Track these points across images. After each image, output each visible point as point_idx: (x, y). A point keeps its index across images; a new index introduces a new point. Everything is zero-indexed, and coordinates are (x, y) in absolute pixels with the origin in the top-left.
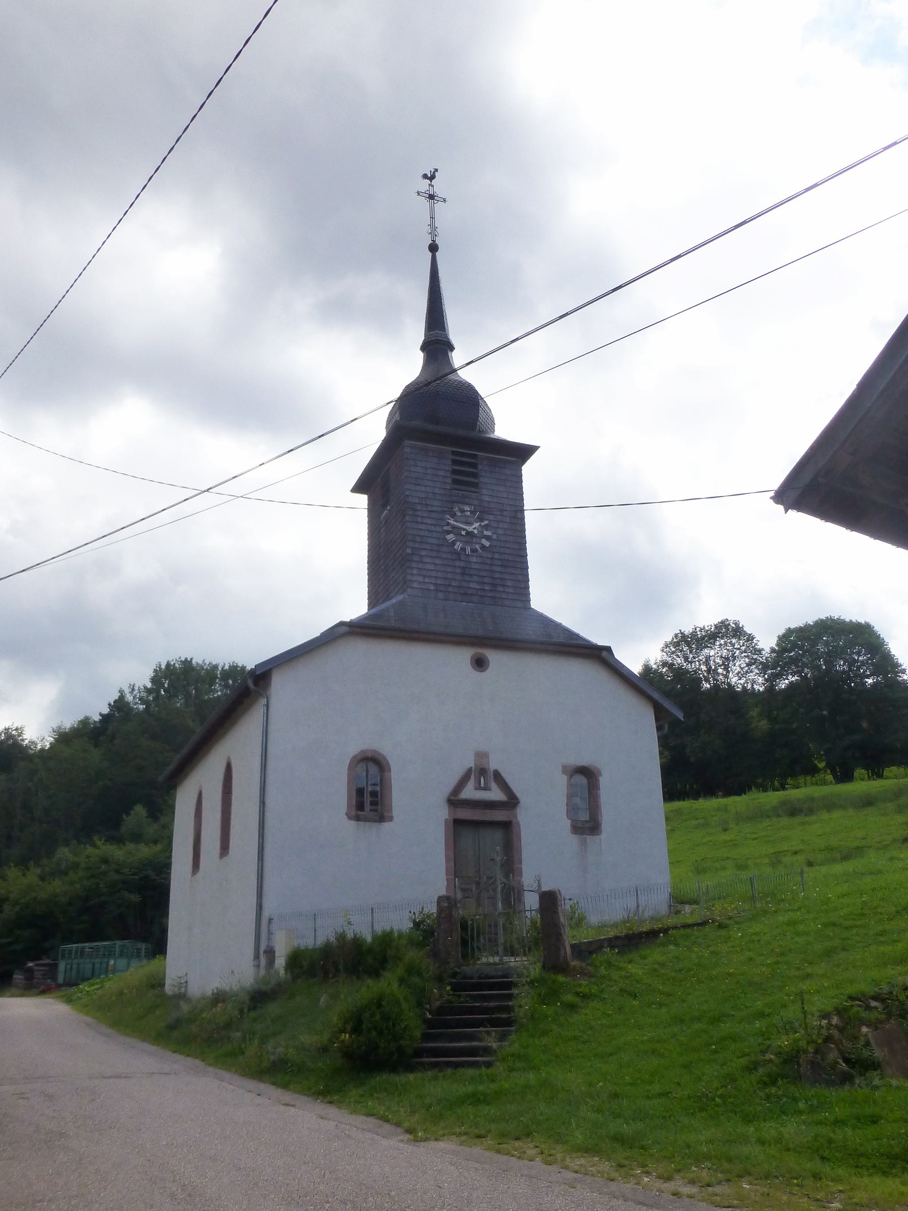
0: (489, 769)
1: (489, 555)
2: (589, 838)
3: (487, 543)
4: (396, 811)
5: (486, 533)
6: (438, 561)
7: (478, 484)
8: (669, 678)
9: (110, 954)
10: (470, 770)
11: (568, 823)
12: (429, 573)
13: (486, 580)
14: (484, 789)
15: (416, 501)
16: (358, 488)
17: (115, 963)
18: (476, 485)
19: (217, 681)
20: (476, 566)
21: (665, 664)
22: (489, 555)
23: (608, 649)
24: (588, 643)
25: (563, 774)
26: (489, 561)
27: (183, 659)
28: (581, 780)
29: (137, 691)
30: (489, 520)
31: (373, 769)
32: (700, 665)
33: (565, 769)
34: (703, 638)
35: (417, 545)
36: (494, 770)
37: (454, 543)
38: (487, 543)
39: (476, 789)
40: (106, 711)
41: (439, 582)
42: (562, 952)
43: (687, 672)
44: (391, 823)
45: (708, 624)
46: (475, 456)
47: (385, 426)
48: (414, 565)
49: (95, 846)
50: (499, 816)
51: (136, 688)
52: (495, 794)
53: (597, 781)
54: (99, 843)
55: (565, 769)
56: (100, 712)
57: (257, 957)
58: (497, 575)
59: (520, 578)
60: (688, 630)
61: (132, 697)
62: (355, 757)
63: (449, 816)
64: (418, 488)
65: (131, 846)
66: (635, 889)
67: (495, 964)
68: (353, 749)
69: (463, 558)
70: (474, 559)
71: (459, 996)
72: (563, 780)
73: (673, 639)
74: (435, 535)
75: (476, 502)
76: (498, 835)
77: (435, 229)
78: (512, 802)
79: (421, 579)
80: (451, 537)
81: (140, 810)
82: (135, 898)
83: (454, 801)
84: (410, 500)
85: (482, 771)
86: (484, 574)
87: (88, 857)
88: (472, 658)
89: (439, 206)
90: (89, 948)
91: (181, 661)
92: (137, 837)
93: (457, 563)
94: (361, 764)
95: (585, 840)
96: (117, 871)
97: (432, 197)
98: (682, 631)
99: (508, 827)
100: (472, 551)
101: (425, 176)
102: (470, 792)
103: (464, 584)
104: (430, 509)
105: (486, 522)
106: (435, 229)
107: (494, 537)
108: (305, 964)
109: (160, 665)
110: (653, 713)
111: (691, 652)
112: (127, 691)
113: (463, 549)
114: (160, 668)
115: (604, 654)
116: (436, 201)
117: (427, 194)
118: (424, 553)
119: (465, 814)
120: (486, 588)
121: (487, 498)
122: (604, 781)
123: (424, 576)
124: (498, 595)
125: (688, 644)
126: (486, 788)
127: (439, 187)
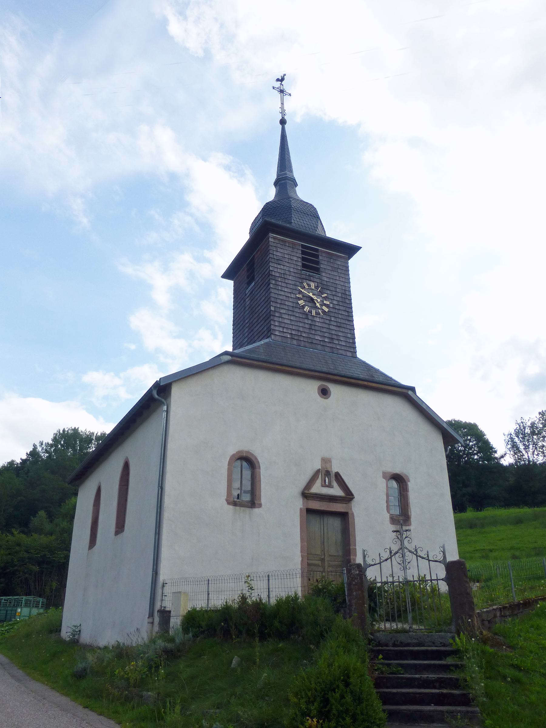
0: (332, 471)
3: (326, 310)
4: (263, 500)
5: (325, 302)
6: (292, 318)
9: (18, 604)
10: (318, 471)
11: (388, 516)
12: (286, 326)
13: (326, 335)
14: (328, 487)
15: (277, 275)
16: (227, 275)
17: (21, 611)
19: (93, 441)
20: (320, 325)
22: (328, 318)
23: (413, 389)
24: (397, 383)
26: (328, 322)
27: (73, 428)
28: (394, 484)
29: (44, 445)
30: (327, 294)
35: (278, 306)
36: (335, 473)
37: (303, 307)
38: (326, 310)
39: (322, 486)
40: (24, 457)
41: (294, 332)
44: (260, 509)
46: (317, 250)
47: (249, 232)
48: (276, 319)
49: (12, 534)
51: (44, 444)
52: (336, 491)
53: (406, 485)
54: (15, 532)
56: (21, 457)
57: (151, 615)
58: (333, 332)
59: (349, 335)
61: (41, 449)
64: (279, 266)
65: (36, 536)
67: (405, 631)
68: (232, 450)
69: (310, 317)
70: (318, 320)
71: (389, 665)
72: (382, 483)
74: (291, 300)
76: (335, 523)
77: (284, 111)
78: (349, 497)
79: (281, 329)
80: (301, 302)
81: (42, 513)
82: (36, 568)
83: (306, 495)
84: (273, 273)
85: (328, 473)
86: (325, 330)
87: (8, 541)
88: (319, 388)
89: (286, 98)
90: (4, 600)
91: (72, 429)
92: (39, 531)
93: (306, 321)
94: (239, 462)
96: (27, 552)
97: (282, 91)
101: (278, 80)
102: (317, 488)
103: (311, 336)
105: (326, 295)
106: (284, 111)
107: (331, 305)
108: (203, 624)
109: (59, 431)
112: (38, 445)
113: (310, 312)
114: (59, 432)
115: (410, 393)
116: (285, 94)
117: (279, 89)
118: (282, 311)
119: (316, 505)
122: (411, 486)
123: (284, 327)
126: (330, 486)
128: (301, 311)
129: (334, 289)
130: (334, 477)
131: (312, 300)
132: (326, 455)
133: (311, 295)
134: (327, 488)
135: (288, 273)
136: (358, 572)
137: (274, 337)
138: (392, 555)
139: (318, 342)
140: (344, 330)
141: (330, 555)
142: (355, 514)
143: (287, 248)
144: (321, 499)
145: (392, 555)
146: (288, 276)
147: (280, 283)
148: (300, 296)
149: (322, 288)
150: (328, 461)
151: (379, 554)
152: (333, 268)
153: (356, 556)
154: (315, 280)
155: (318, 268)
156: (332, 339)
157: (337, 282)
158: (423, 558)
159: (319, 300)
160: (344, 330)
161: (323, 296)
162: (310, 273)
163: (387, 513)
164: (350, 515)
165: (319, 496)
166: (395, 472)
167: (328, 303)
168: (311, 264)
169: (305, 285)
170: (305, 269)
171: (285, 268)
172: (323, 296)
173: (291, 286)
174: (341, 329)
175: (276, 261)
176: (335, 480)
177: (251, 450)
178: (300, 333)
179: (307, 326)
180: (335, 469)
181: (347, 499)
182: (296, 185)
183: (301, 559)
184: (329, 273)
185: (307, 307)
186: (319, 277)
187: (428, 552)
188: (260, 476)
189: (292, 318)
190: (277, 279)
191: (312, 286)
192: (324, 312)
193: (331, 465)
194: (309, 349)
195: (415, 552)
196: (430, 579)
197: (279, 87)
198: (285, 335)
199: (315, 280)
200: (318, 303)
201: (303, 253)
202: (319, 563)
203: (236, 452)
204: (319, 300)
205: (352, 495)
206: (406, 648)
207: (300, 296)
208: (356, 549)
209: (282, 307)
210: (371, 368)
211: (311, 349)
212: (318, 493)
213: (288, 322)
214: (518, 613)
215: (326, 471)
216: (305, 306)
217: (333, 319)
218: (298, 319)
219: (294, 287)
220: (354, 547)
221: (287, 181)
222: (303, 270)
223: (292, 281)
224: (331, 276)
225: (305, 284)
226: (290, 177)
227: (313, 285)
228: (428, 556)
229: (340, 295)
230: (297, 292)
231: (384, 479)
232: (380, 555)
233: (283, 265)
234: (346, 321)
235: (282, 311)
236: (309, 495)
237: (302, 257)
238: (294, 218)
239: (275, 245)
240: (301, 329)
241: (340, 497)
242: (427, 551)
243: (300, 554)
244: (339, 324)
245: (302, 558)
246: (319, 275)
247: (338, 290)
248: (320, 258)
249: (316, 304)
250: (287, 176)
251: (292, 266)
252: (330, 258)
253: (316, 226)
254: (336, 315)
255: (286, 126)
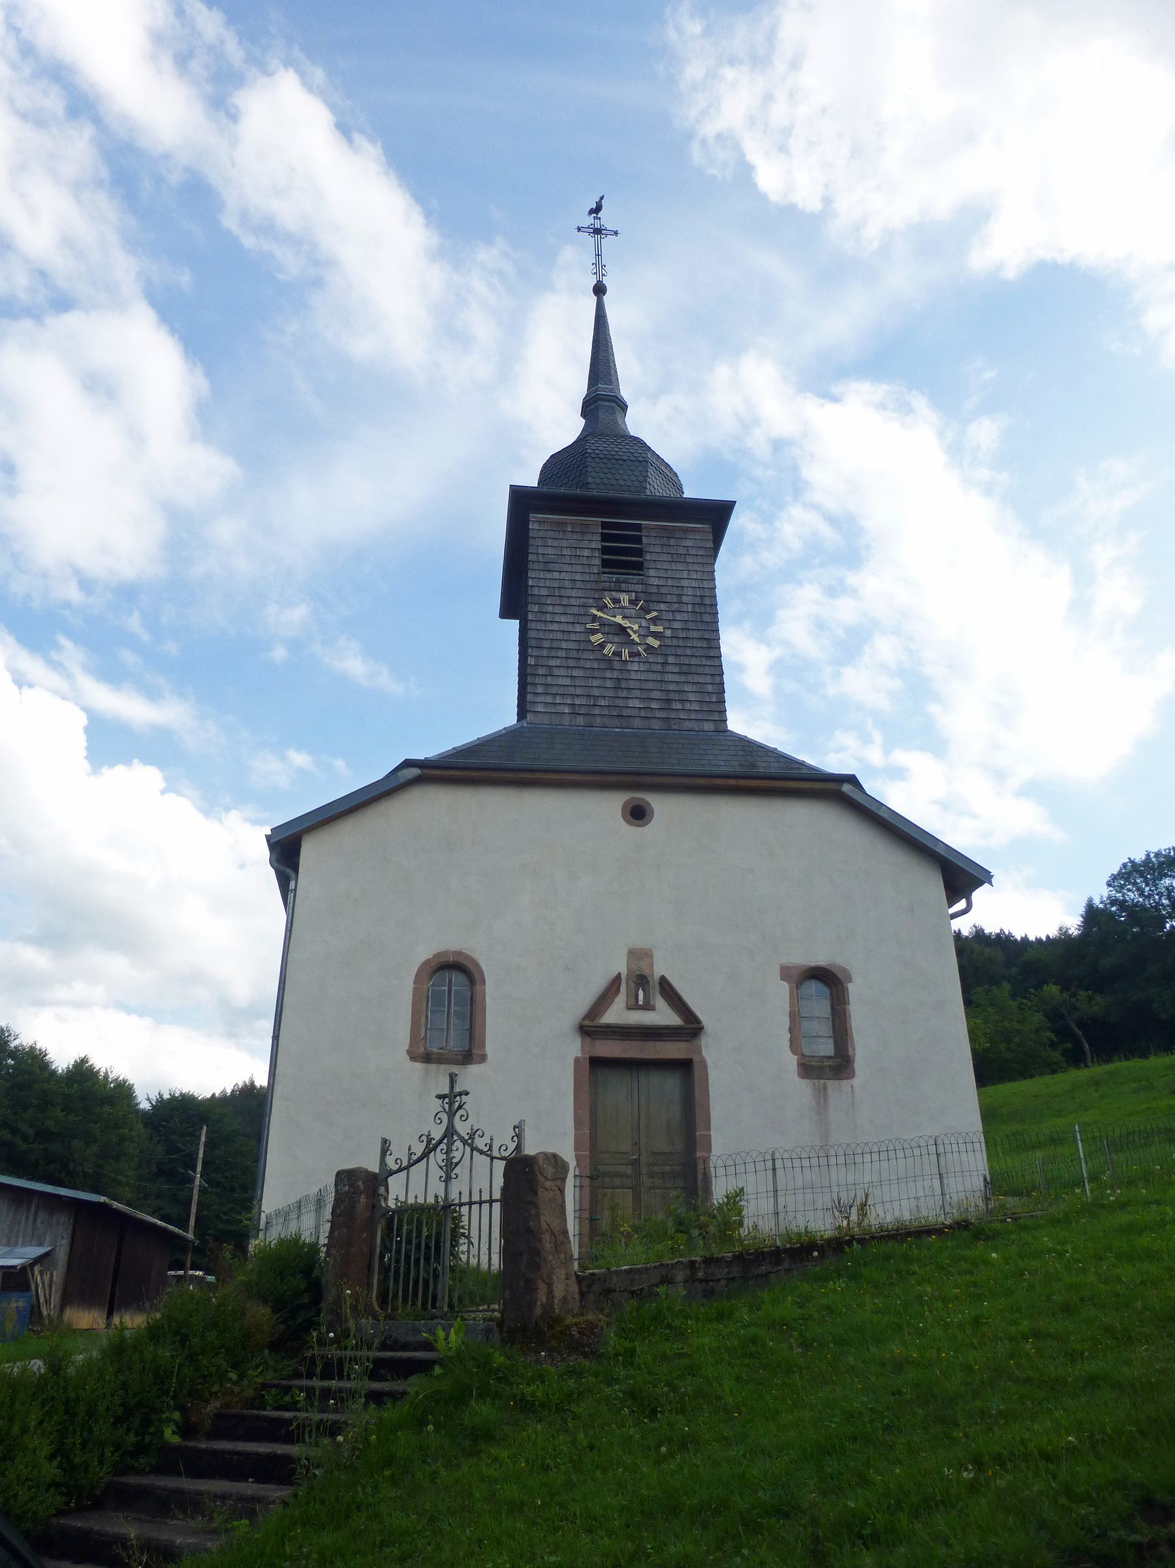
1: (660, 660)
2: (831, 1084)
3: (655, 643)
4: (490, 1048)
5: (653, 628)
7: (642, 563)
8: (1122, 919)
10: (618, 978)
11: (793, 1061)
13: (655, 694)
15: (544, 592)
18: (639, 566)
21: (1114, 902)
22: (660, 660)
23: (852, 780)
25: (781, 980)
26: (659, 668)
31: (457, 978)
32: (1160, 899)
33: (786, 973)
34: (1161, 864)
35: (545, 653)
37: (602, 646)
38: (655, 643)
39: (629, 1008)
41: (577, 702)
42: (542, 1297)
43: (1143, 906)
45: (1166, 848)
46: (638, 527)
48: (538, 680)
50: (671, 1050)
52: (663, 1015)
55: (786, 973)
60: (1139, 857)
62: (426, 963)
63: (582, 1054)
64: (549, 575)
66: (769, 1157)
68: (424, 953)
69: (617, 665)
72: (781, 992)
73: (1121, 869)
75: (639, 588)
76: (671, 1083)
78: (691, 1028)
79: (549, 699)
80: (597, 638)
83: (589, 1029)
85: (641, 980)
86: (650, 686)
89: (607, 242)
93: (608, 674)
95: (825, 1088)
98: (1132, 859)
99: (685, 1067)
100: (631, 655)
102: (617, 1014)
103: (620, 703)
104: (565, 602)
105: (655, 614)
110: (941, 875)
111: (1147, 885)
115: (846, 788)
118: (553, 663)
119: (610, 1049)
120: (654, 705)
121: (656, 582)
122: (854, 990)
124: (673, 715)
125: (1142, 875)
126: (648, 1007)
127: (607, 219)
128: (597, 655)
129: (675, 599)
130: (657, 987)
131: (623, 630)
132: (640, 943)
133: (618, 619)
134: (640, 1011)
135: (567, 584)
136: (347, 1188)
137: (533, 717)
138: (430, 1149)
139: (635, 712)
140: (697, 679)
141: (653, 1153)
143: (569, 536)
145: (430, 1149)
146: (570, 591)
147: (550, 609)
148: (596, 625)
149: (646, 601)
151: (410, 1146)
152: (675, 555)
153: (710, 1151)
154: (631, 587)
155: (639, 562)
156: (669, 701)
157: (685, 583)
158: (481, 1152)
159: (636, 627)
160: (697, 679)
161: (648, 617)
162: (619, 576)
163: (792, 1055)
164: (697, 1067)
166: (813, 964)
167: (660, 629)
168: (629, 558)
169: (607, 602)
170: (607, 570)
171: (563, 575)
172: (648, 617)
173: (575, 610)
174: (690, 678)
175: (541, 566)
177: (464, 949)
178: (592, 700)
179: (609, 684)
180: (660, 969)
181: (685, 1031)
182: (624, 407)
184: (665, 568)
185: (609, 645)
186: (641, 581)
187: (492, 1139)
188: (485, 999)
189: (575, 673)
190: (543, 600)
191: (622, 602)
192: (649, 648)
193: (652, 962)
194: (612, 730)
195: (469, 1142)
196: (489, 1199)
197: (592, 224)
198: (559, 709)
199: (631, 587)
200: (635, 632)
201: (605, 538)
202: (629, 1170)
203: (433, 956)
204: (636, 627)
205: (698, 1021)
206: (399, 1354)
207: (596, 625)
208: (710, 1135)
209: (553, 654)
210: (755, 749)
211: (616, 730)
213: (567, 681)
214: (770, 1273)
215: (639, 975)
216: (605, 644)
217: (671, 660)
218: (589, 673)
219: (582, 611)
220: (706, 1133)
221: (600, 403)
222: (604, 573)
223: (578, 600)
224: (669, 574)
225: (607, 600)
226: (605, 393)
227: (625, 598)
228: (490, 1149)
229: (690, 608)
230: (589, 619)
232: (409, 1149)
233: (557, 571)
234: (704, 659)
235: (553, 663)
236: (593, 1029)
237: (602, 546)
238: (593, 474)
239: (541, 534)
240: (596, 692)
241: (668, 1028)
242: (491, 1137)
243: (574, 1154)
244: (685, 669)
245: (577, 1162)
246: (643, 575)
247: (685, 599)
248: (645, 540)
249: (631, 636)
250: (598, 392)
251: (579, 569)
252: (669, 538)
253: (641, 479)
254: (679, 651)
255: (606, 298)
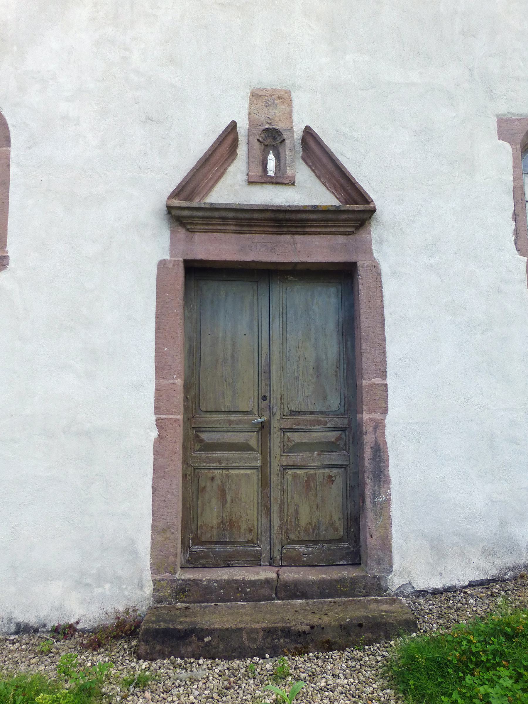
14: (272, 183)
39: (251, 183)
134: (270, 187)
141: (292, 413)
142: (385, 268)
144: (242, 226)
150: (279, 98)
153: (385, 410)
165: (231, 215)
176: (303, 159)
181: (344, 216)
183: (155, 434)
202: (252, 439)
212: (220, 204)
215: (267, 130)
231: (503, 140)
